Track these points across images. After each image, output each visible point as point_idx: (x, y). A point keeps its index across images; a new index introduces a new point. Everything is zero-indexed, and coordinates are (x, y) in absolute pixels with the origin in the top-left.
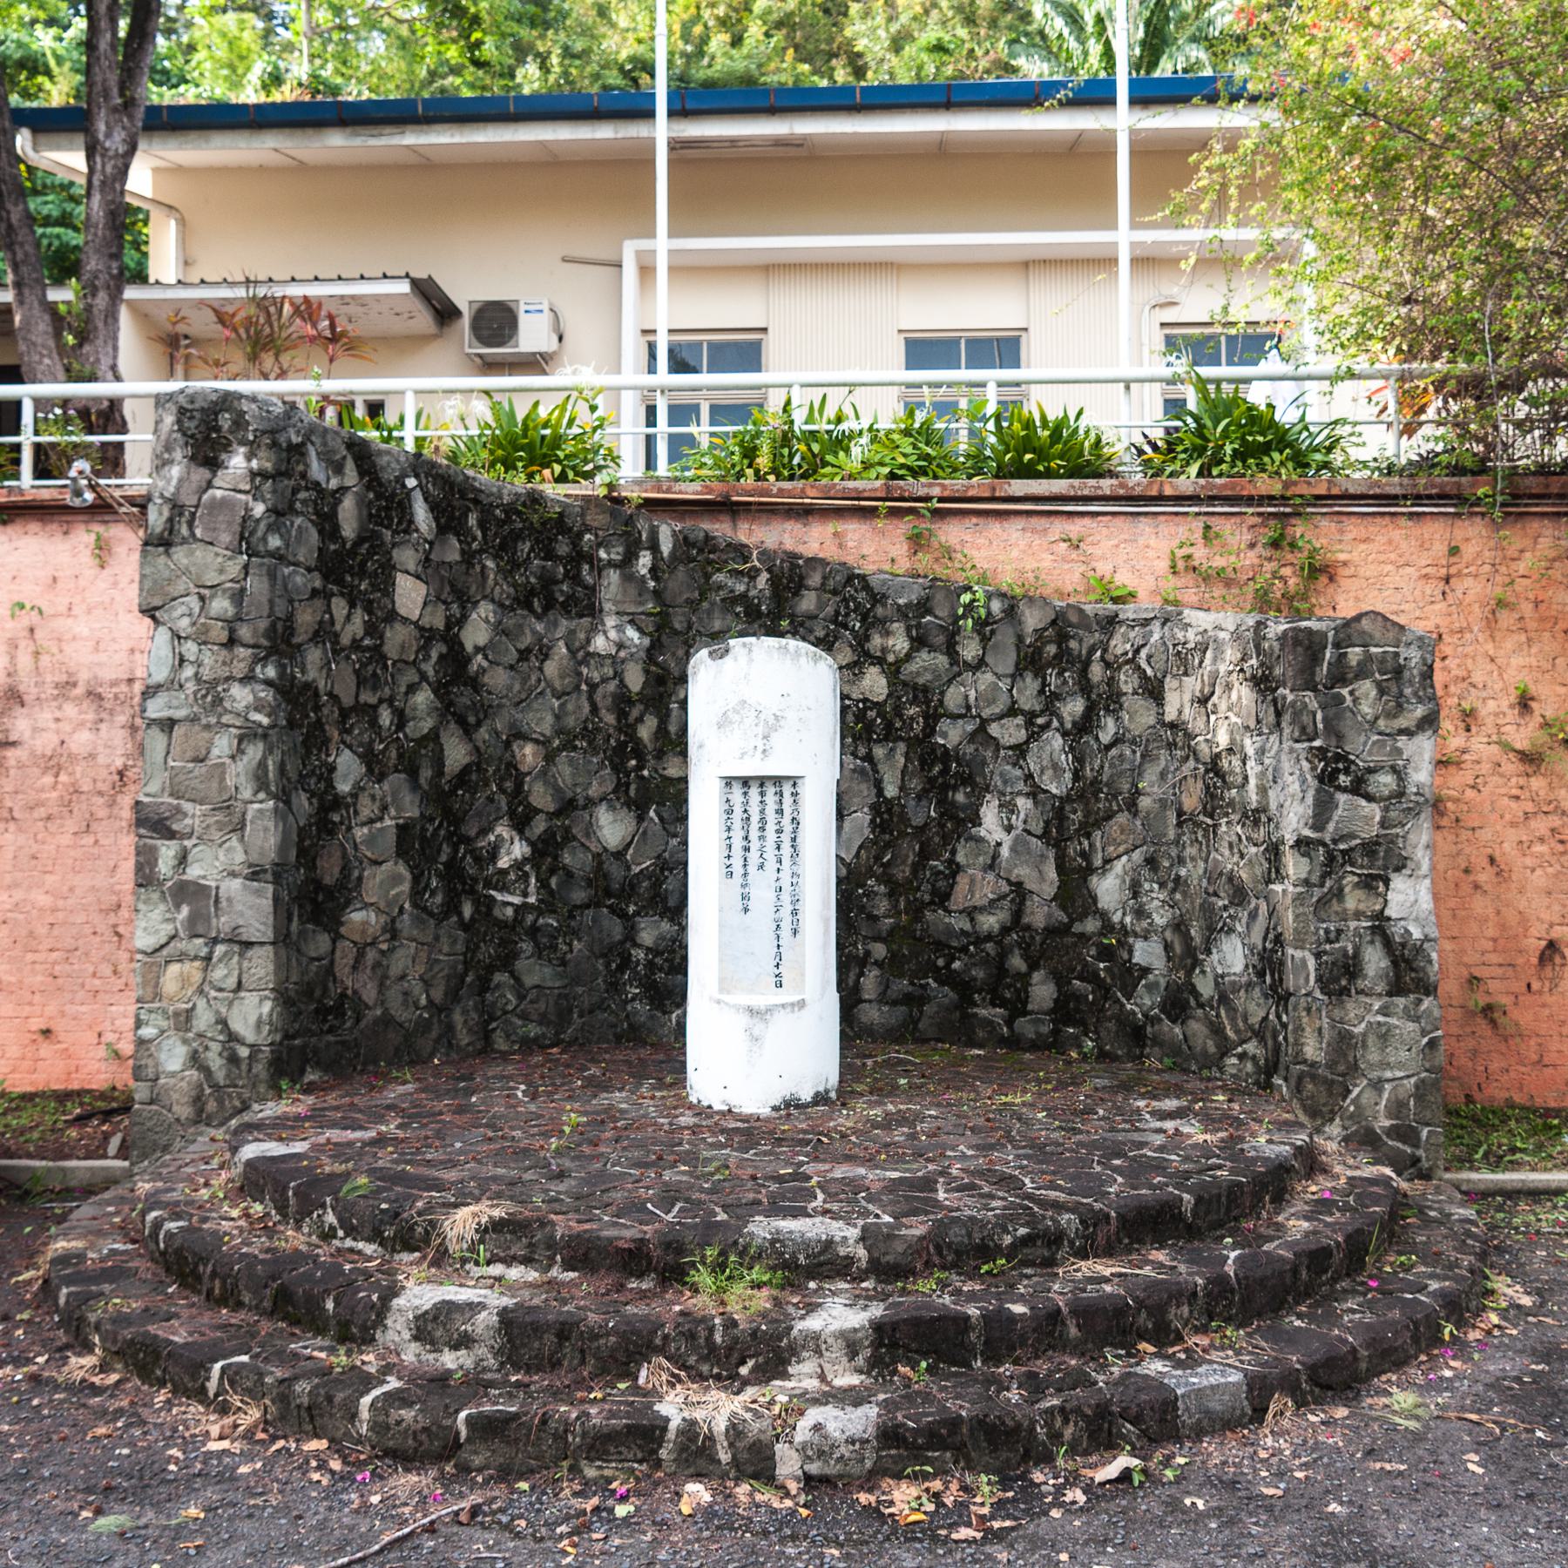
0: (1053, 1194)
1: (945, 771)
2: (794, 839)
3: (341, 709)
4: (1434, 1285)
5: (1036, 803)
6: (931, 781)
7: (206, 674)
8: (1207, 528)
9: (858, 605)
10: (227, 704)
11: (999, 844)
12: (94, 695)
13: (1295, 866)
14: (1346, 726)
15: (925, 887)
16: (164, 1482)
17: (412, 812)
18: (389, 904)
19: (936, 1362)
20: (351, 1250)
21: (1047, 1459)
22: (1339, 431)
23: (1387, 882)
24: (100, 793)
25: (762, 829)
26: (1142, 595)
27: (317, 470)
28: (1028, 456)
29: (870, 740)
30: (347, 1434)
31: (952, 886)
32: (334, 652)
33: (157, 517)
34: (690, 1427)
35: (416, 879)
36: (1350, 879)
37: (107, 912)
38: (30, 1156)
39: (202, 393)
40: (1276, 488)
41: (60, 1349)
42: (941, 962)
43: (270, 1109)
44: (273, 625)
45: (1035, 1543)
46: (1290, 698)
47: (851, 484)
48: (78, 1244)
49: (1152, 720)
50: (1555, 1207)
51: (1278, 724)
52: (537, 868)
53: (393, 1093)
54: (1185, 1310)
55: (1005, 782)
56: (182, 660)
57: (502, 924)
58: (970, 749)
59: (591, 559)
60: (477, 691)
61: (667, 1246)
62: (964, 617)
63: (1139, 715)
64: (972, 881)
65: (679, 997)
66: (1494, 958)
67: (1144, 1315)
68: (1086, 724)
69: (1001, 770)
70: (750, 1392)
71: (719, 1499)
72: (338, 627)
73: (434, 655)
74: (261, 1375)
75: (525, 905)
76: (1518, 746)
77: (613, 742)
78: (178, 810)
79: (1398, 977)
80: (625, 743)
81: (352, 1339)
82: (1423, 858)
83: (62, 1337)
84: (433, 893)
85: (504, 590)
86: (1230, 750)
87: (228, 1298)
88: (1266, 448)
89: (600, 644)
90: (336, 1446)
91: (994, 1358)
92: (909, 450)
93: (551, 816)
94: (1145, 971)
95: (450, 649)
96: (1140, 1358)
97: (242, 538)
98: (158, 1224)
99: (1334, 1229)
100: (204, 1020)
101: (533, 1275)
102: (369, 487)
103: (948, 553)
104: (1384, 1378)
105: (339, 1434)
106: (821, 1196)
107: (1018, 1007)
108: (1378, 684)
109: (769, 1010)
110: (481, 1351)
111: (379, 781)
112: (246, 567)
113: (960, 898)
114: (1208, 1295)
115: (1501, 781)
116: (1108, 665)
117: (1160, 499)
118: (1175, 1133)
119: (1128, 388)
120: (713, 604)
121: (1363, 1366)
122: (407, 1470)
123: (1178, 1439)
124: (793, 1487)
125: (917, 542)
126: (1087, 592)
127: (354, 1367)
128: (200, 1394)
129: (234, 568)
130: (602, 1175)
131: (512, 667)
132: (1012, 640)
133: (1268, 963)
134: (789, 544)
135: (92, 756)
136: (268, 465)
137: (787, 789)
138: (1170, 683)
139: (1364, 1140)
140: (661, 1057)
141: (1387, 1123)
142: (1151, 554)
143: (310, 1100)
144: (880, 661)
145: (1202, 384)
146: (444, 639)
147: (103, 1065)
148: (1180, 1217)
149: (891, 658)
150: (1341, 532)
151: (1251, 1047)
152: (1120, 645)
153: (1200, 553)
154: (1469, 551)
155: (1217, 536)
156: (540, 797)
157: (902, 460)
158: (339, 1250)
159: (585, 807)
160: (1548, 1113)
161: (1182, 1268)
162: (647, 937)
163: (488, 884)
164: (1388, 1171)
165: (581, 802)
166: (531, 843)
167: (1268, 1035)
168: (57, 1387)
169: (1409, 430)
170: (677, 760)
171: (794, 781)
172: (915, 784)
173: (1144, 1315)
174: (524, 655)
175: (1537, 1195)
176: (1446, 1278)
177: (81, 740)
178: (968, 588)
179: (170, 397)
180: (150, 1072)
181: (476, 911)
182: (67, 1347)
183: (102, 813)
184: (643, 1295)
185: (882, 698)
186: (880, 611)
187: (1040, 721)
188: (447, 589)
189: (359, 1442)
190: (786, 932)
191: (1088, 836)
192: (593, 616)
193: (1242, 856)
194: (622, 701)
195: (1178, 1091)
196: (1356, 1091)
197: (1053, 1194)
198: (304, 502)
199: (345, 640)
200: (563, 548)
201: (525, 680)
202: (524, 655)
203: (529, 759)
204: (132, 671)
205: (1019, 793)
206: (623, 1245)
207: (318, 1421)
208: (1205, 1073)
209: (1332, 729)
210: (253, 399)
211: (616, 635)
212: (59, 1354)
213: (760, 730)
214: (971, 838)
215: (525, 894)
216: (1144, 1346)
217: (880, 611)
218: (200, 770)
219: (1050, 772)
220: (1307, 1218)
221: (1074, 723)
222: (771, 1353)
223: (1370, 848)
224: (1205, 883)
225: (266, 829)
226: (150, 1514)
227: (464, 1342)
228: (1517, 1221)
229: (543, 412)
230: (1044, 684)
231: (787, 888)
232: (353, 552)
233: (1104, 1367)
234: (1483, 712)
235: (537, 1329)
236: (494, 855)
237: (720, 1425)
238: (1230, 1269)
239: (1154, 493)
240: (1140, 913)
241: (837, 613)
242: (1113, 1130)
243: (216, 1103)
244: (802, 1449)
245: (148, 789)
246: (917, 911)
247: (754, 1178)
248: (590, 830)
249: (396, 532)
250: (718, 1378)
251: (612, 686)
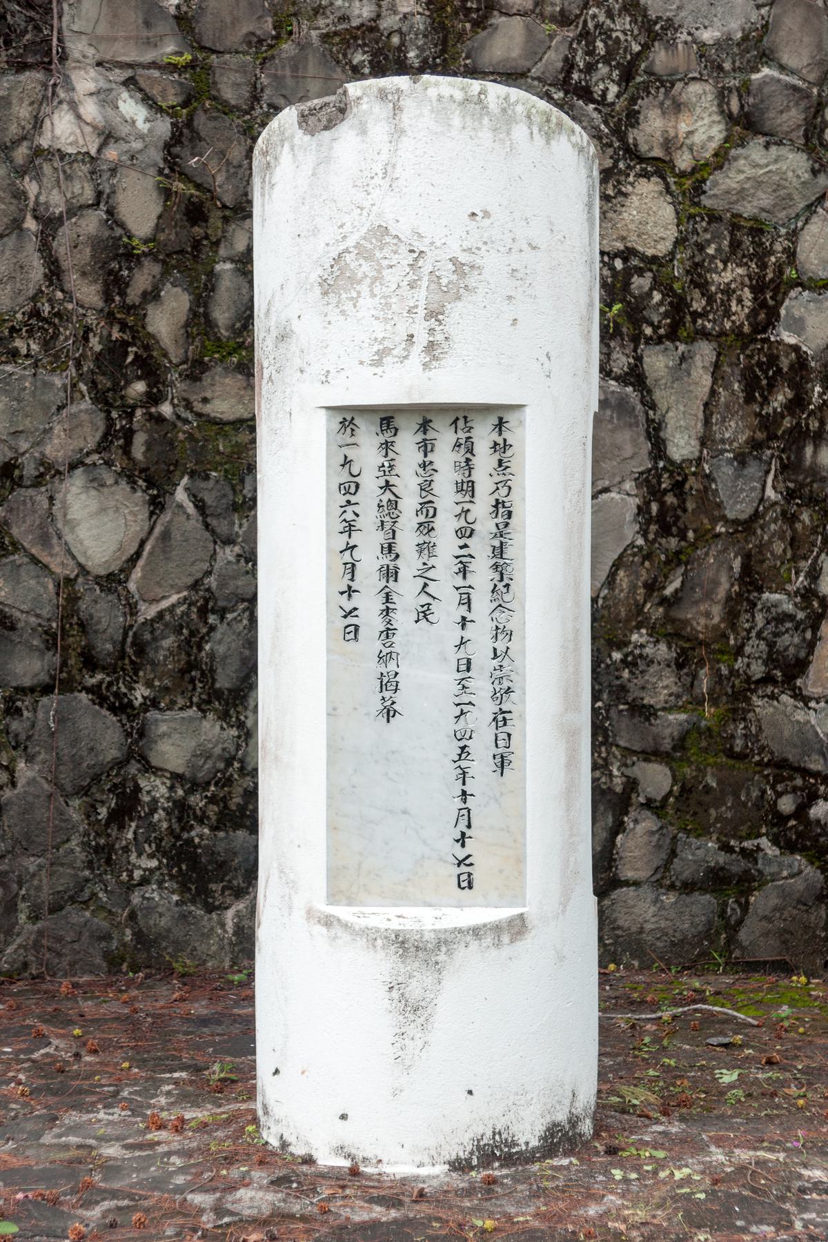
1: (798, 403)
2: (499, 551)
6: (768, 424)
9: (614, 48)
15: (755, 647)
25: (426, 527)
29: (636, 339)
31: (811, 646)
42: (786, 804)
65: (242, 876)
77: (95, 344)
80: (125, 344)
89: (62, 130)
109: (446, 941)
137: (483, 436)
140: (199, 1008)
144: (659, 168)
149: (684, 161)
159: (38, 481)
165: (30, 470)
170: (232, 382)
171: (500, 416)
172: (735, 431)
185: (663, 249)
186: (660, 58)
192: (46, 67)
194: (115, 257)
213: (421, 296)
217: (660, 58)
241: (569, 65)
246: (737, 698)
251: (91, 223)
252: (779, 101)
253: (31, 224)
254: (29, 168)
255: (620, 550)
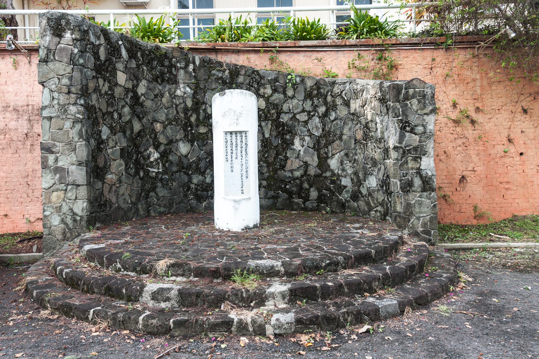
0: (333, 251)
1: (283, 129)
2: (246, 150)
3: (103, 113)
4: (445, 275)
5: (311, 138)
6: (279, 132)
7: (61, 102)
8: (359, 54)
10: (69, 112)
11: (300, 151)
12: (16, 110)
13: (393, 155)
14: (409, 113)
16: (82, 345)
17: (125, 145)
18: (118, 172)
19: (308, 300)
20: (126, 275)
21: (344, 327)
22: (397, 24)
23: (421, 159)
24: (20, 141)
25: (236, 147)
26: (340, 75)
27: (92, 39)
28: (305, 33)
30: (136, 328)
31: (286, 163)
32: (100, 95)
33: (42, 53)
34: (240, 322)
35: (126, 165)
36: (410, 158)
37: (24, 178)
38: (9, 254)
39: (55, 13)
40: (380, 42)
41: (36, 309)
42: (283, 186)
43: (88, 235)
44: (82, 87)
45: (346, 351)
46: (392, 105)
47: (252, 43)
48: (35, 278)
49: (346, 113)
50: (471, 253)
51: (388, 113)
52: (162, 160)
53: (124, 229)
54: (377, 283)
55: (301, 132)
56: (53, 98)
57: (152, 178)
58: (291, 123)
59: (175, 66)
60: (142, 107)
61: (225, 269)
62: (289, 83)
63: (342, 112)
64: (292, 162)
66: (446, 181)
67: (366, 285)
68: (326, 114)
69: (300, 129)
70: (255, 311)
71: (251, 341)
72: (101, 88)
73: (129, 96)
74: (106, 312)
75: (159, 172)
76: (453, 118)
78: (54, 145)
79: (424, 186)
80: (187, 123)
81: (131, 300)
82: (431, 152)
83: (36, 305)
84: (131, 169)
85: (149, 76)
86: (371, 121)
87: (89, 291)
88: (376, 30)
89: (179, 93)
90: (132, 332)
91: (324, 298)
92: (268, 32)
93: (166, 145)
94: (345, 187)
95: (134, 94)
96: (366, 297)
97: (71, 60)
98: (62, 271)
99: (414, 260)
100: (65, 209)
101: (184, 279)
102: (108, 44)
103: (282, 64)
104: (435, 302)
105: (132, 329)
106: (266, 254)
107: (306, 199)
108: (418, 100)
109: (240, 201)
110: (173, 302)
111: (114, 135)
112: (73, 69)
113: (288, 166)
114: (383, 279)
115: (448, 129)
116: (333, 96)
117: (345, 46)
118: (363, 234)
119: (333, 12)
120: (212, 80)
121: (429, 298)
122: (155, 338)
123: (380, 320)
124: (272, 337)
125: (272, 60)
126: (323, 75)
127: (134, 309)
128: (86, 319)
129: (69, 69)
130: (198, 250)
131: (152, 100)
132: (303, 89)
133: (385, 184)
134: (234, 62)
135: (16, 129)
136: (78, 37)
137: (244, 135)
138: (352, 102)
139: (415, 234)
140: (201, 216)
141: (422, 229)
142: (342, 63)
143: (100, 232)
144: (263, 97)
145: (356, 10)
146: (132, 91)
147: (25, 225)
148: (371, 257)
149: (266, 96)
150: (400, 55)
151: (379, 208)
152: (336, 90)
153: (357, 63)
154: (438, 60)
155: (362, 57)
156: (162, 139)
157: (266, 35)
158: (123, 275)
159: (175, 142)
160: (463, 226)
161: (374, 271)
162: (195, 181)
163: (147, 166)
164: (424, 243)
165: (174, 141)
166: (160, 153)
167: (385, 205)
168: (38, 320)
169: (418, 23)
171: (246, 132)
172: (274, 133)
173: (366, 285)
174: (156, 96)
175: (465, 249)
176: (448, 273)
177: (12, 124)
178: (289, 74)
179: (44, 14)
180: (49, 226)
181: (144, 174)
182: (38, 308)
183: (21, 147)
184: (219, 284)
185: (264, 108)
187: (312, 114)
188: (133, 76)
189: (139, 330)
190: (244, 177)
191: (327, 147)
193: (376, 152)
194: (186, 110)
195: (358, 222)
196: (412, 220)
197: (333, 251)
198: (89, 48)
199: (103, 92)
200: (166, 63)
201: (156, 104)
202: (156, 96)
203: (159, 128)
204: (28, 102)
205: (306, 135)
206: (212, 269)
207: (126, 325)
208: (365, 216)
209: (404, 114)
210: (72, 15)
211: (183, 90)
212: (37, 310)
213: (235, 117)
214: (291, 149)
215: (158, 169)
216: (366, 294)
217: (263, 81)
218: (61, 132)
219: (315, 129)
220: (405, 257)
221: (322, 114)
222: (260, 299)
223: (416, 149)
224: (363, 160)
225: (83, 150)
226: (81, 355)
227: (168, 299)
228: (461, 257)
229: (154, 21)
230: (313, 103)
231: (244, 164)
232: (104, 65)
233: (356, 300)
234: (442, 108)
235: (190, 295)
236: (149, 157)
237: (249, 320)
238: (388, 271)
239: (343, 44)
240: (343, 170)
241: (250, 82)
242: (343, 233)
243: (68, 234)
244: (273, 326)
245: (44, 139)
246: (275, 171)
247: (244, 249)
248: (177, 149)
249: (116, 58)
250: (245, 307)
251: (182, 105)
252: (279, 88)
253: (174, 106)
254: (174, 98)
255: (411, 78)
